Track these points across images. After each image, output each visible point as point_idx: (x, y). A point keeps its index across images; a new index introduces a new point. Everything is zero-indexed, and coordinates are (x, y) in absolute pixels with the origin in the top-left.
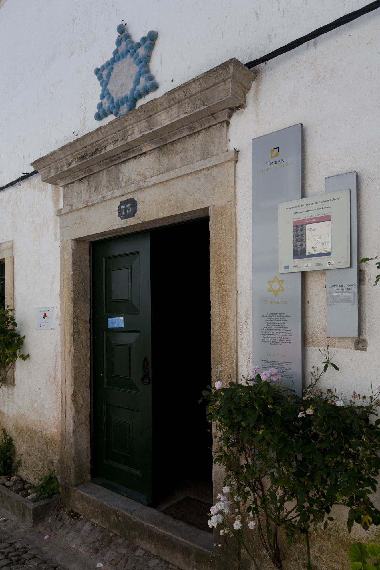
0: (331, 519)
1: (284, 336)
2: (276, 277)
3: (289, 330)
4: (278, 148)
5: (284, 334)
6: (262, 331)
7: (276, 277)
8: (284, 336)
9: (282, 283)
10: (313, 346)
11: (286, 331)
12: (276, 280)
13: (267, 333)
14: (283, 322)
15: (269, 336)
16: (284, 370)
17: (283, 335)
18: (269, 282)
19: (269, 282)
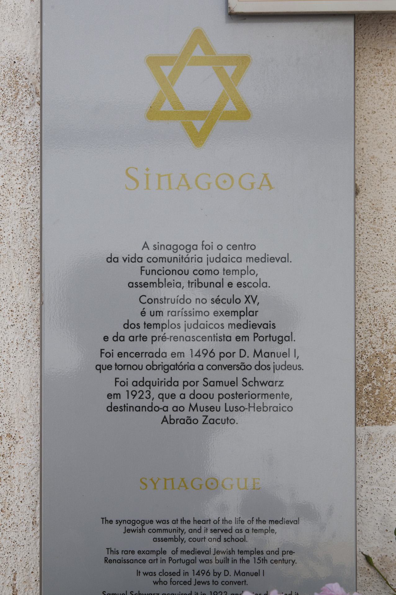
0: (146, 246)
1: (250, 375)
2: (198, 36)
3: (281, 340)
4: (203, 423)
5: (252, 361)
6: (110, 346)
7: (198, 36)
8: (250, 375)
9: (238, 75)
10: (380, 421)
11: (259, 345)
12: (198, 52)
13: (145, 361)
14: (241, 293)
15: (159, 375)
16: (252, 567)
17: (243, 367)
18: (154, 62)
19: (154, 62)
